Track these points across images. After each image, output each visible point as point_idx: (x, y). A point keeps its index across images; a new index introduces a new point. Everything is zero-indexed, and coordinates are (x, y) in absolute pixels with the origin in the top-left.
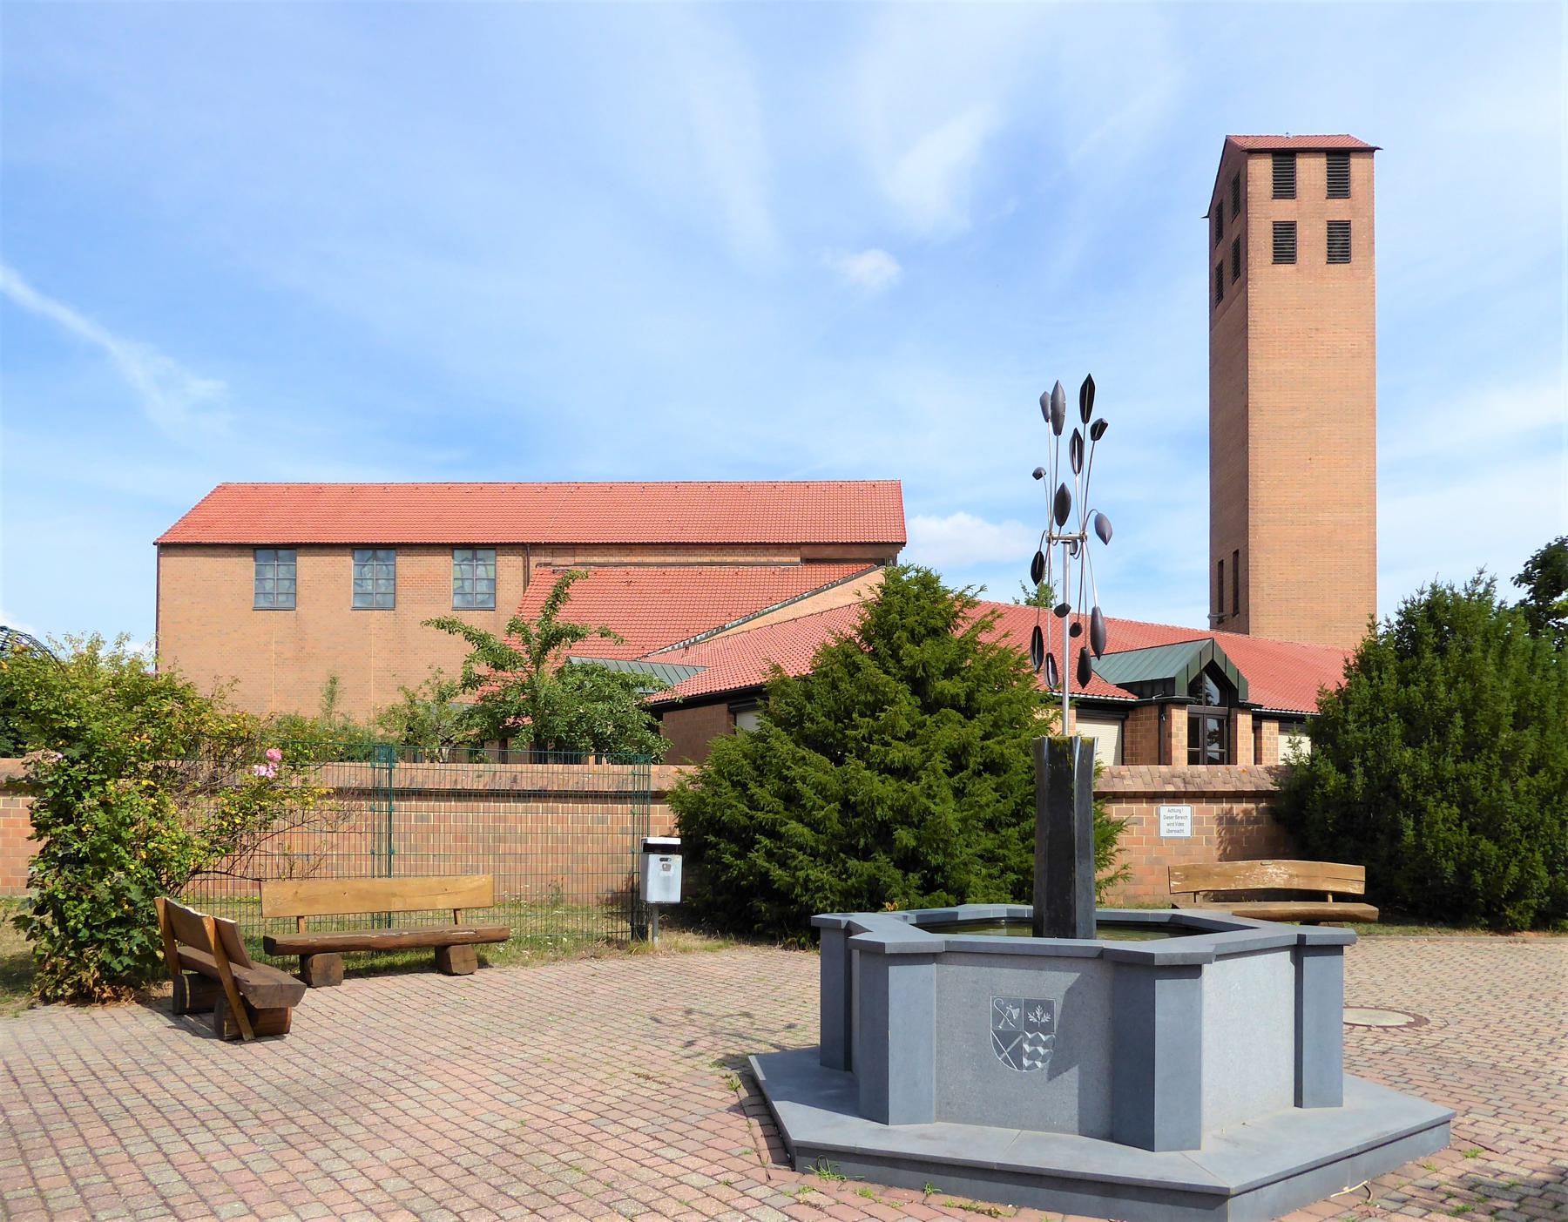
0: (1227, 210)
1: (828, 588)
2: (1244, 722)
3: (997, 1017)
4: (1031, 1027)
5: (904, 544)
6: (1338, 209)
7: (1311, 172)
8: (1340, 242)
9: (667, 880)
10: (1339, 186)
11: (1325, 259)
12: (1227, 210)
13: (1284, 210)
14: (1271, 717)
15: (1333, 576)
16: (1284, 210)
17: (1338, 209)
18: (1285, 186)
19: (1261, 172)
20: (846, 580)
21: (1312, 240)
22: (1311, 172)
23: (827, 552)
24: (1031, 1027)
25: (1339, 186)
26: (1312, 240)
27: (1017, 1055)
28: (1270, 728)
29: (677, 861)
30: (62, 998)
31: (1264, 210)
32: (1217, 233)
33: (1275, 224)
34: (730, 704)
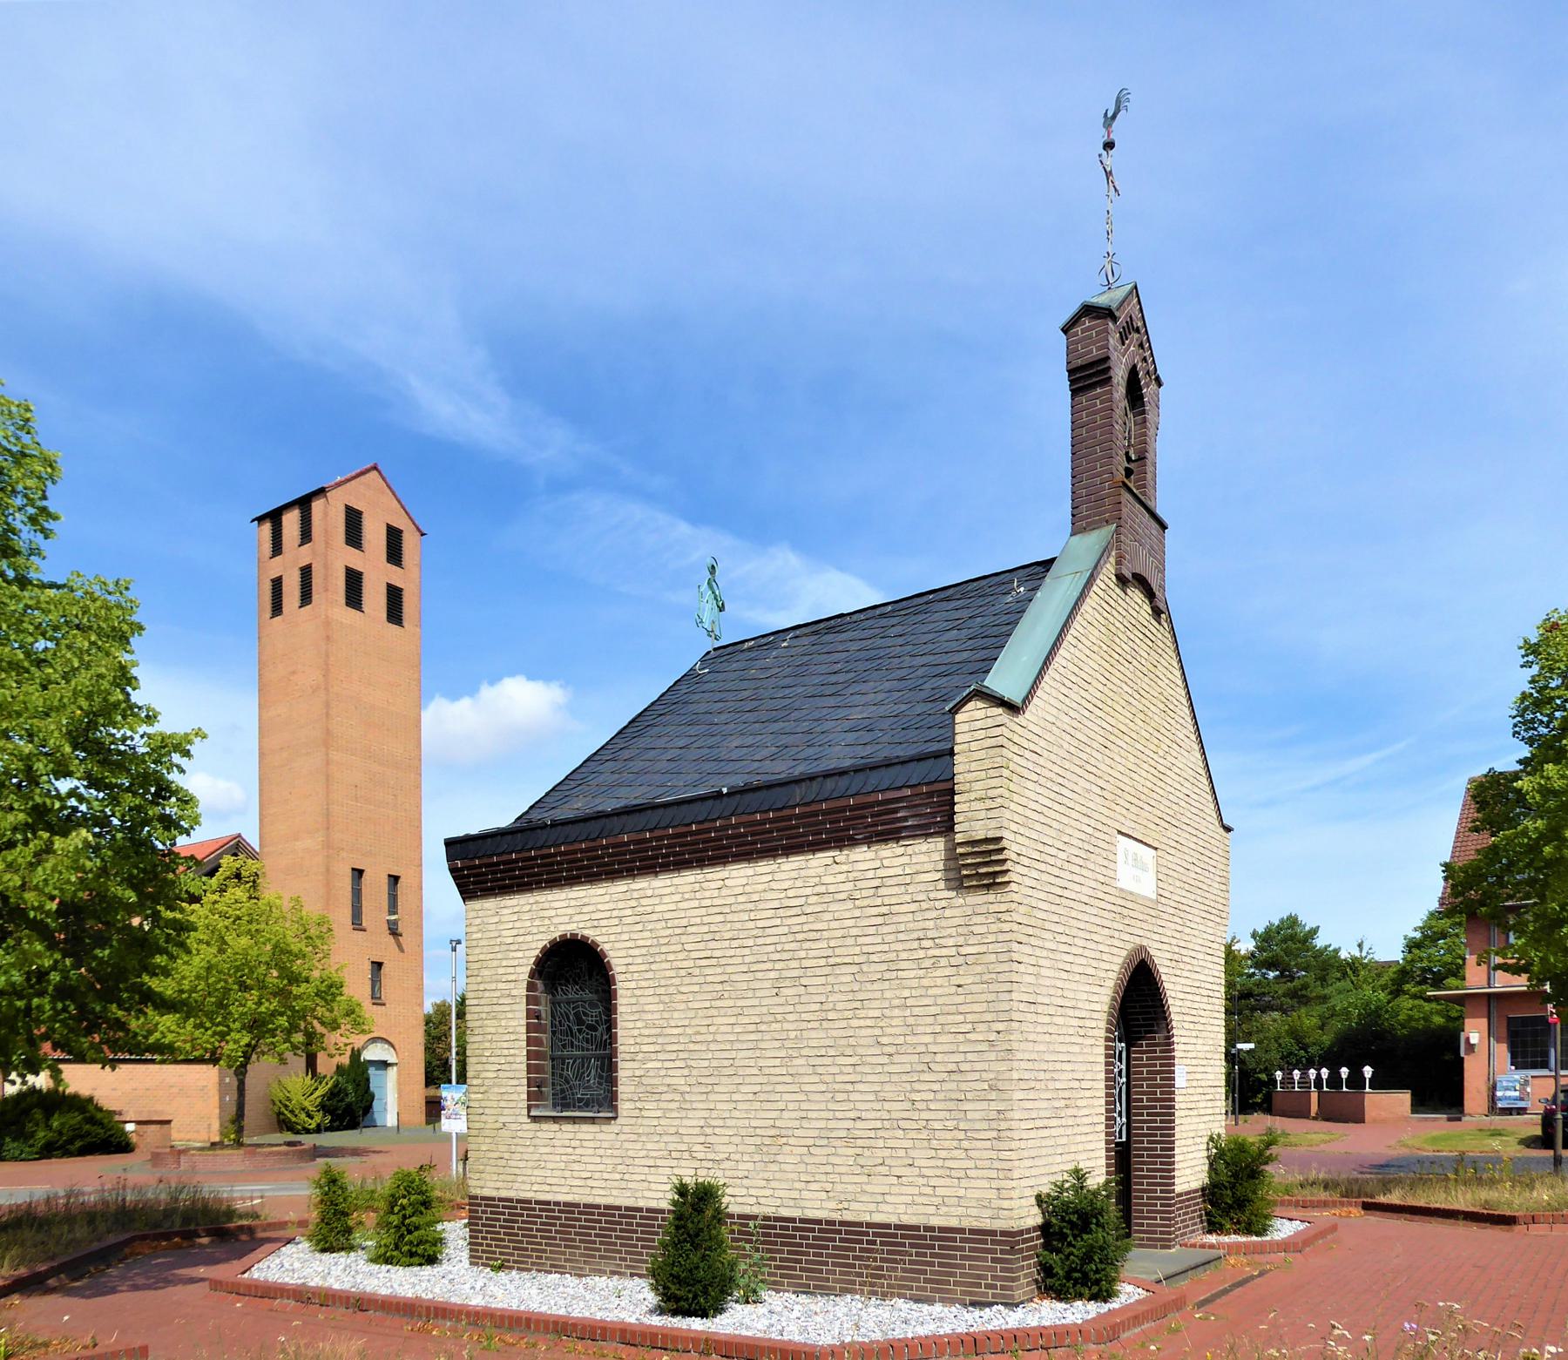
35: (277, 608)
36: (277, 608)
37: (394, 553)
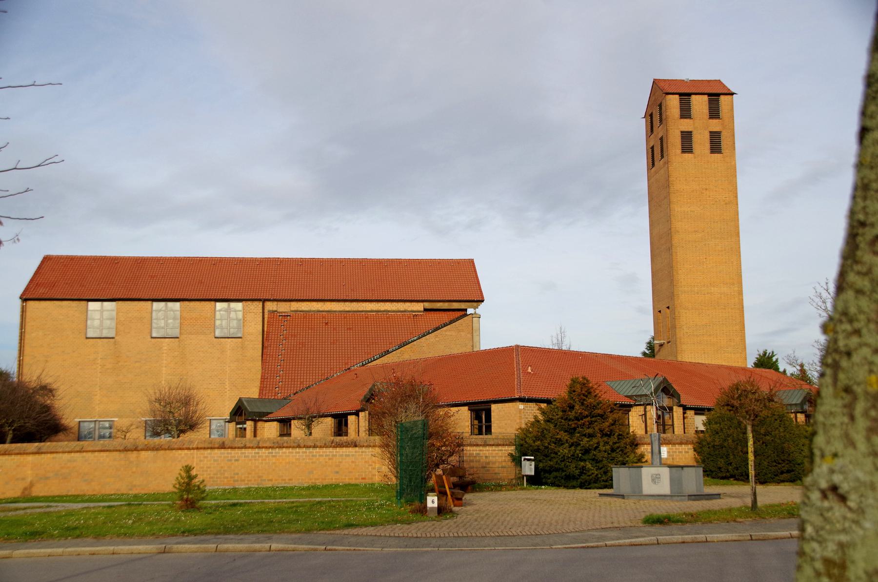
0: (656, 118)
1: (442, 327)
2: (678, 412)
3: (652, 477)
4: (657, 478)
5: (483, 301)
6: (715, 125)
7: (700, 104)
8: (716, 143)
9: (531, 469)
10: (714, 113)
11: (709, 151)
12: (656, 118)
13: (686, 125)
14: (690, 409)
15: (721, 323)
16: (686, 125)
17: (715, 125)
18: (686, 112)
19: (673, 102)
20: (451, 322)
21: (701, 141)
22: (700, 104)
23: (438, 305)
24: (657, 478)
25: (714, 113)
26: (701, 141)
27: (655, 482)
28: (690, 413)
29: (533, 463)
30: (161, 535)
31: (677, 126)
32: (651, 129)
33: (682, 132)
34: (469, 407)
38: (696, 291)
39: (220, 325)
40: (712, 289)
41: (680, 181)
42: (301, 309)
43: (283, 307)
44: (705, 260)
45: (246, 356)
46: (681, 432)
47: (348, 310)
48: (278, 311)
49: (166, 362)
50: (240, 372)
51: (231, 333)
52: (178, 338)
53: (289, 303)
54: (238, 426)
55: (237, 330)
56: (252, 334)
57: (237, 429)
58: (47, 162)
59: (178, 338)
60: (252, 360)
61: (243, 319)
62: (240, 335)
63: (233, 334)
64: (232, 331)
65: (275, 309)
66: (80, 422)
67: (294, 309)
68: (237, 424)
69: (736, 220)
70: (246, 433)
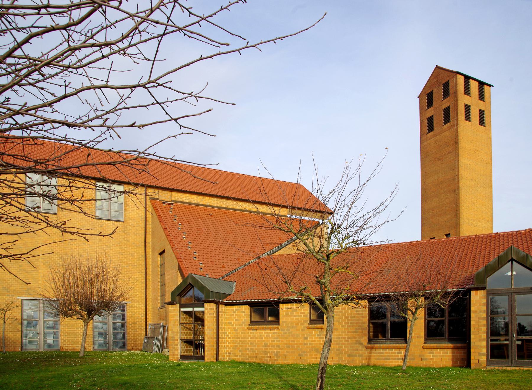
7: (474, 86)
17: (481, 105)
25: (481, 97)
35: (431, 128)
36: (431, 128)
37: (481, 97)
38: (471, 223)
39: (100, 206)
40: (479, 223)
41: (464, 140)
42: (181, 200)
43: (165, 196)
44: (475, 201)
45: (128, 241)
46: (222, 310)
47: (224, 206)
48: (160, 199)
49: (43, 238)
50: (122, 256)
51: (112, 216)
52: (56, 214)
53: (170, 193)
54: (183, 309)
55: (118, 213)
56: (134, 219)
57: (180, 312)
58: (29, 231)
59: (56, 214)
60: (134, 245)
61: (125, 203)
62: (121, 219)
63: (114, 216)
64: (113, 213)
65: (156, 197)
66: (22, 299)
67: (175, 199)
68: (182, 306)
69: (491, 176)
70: (204, 329)
